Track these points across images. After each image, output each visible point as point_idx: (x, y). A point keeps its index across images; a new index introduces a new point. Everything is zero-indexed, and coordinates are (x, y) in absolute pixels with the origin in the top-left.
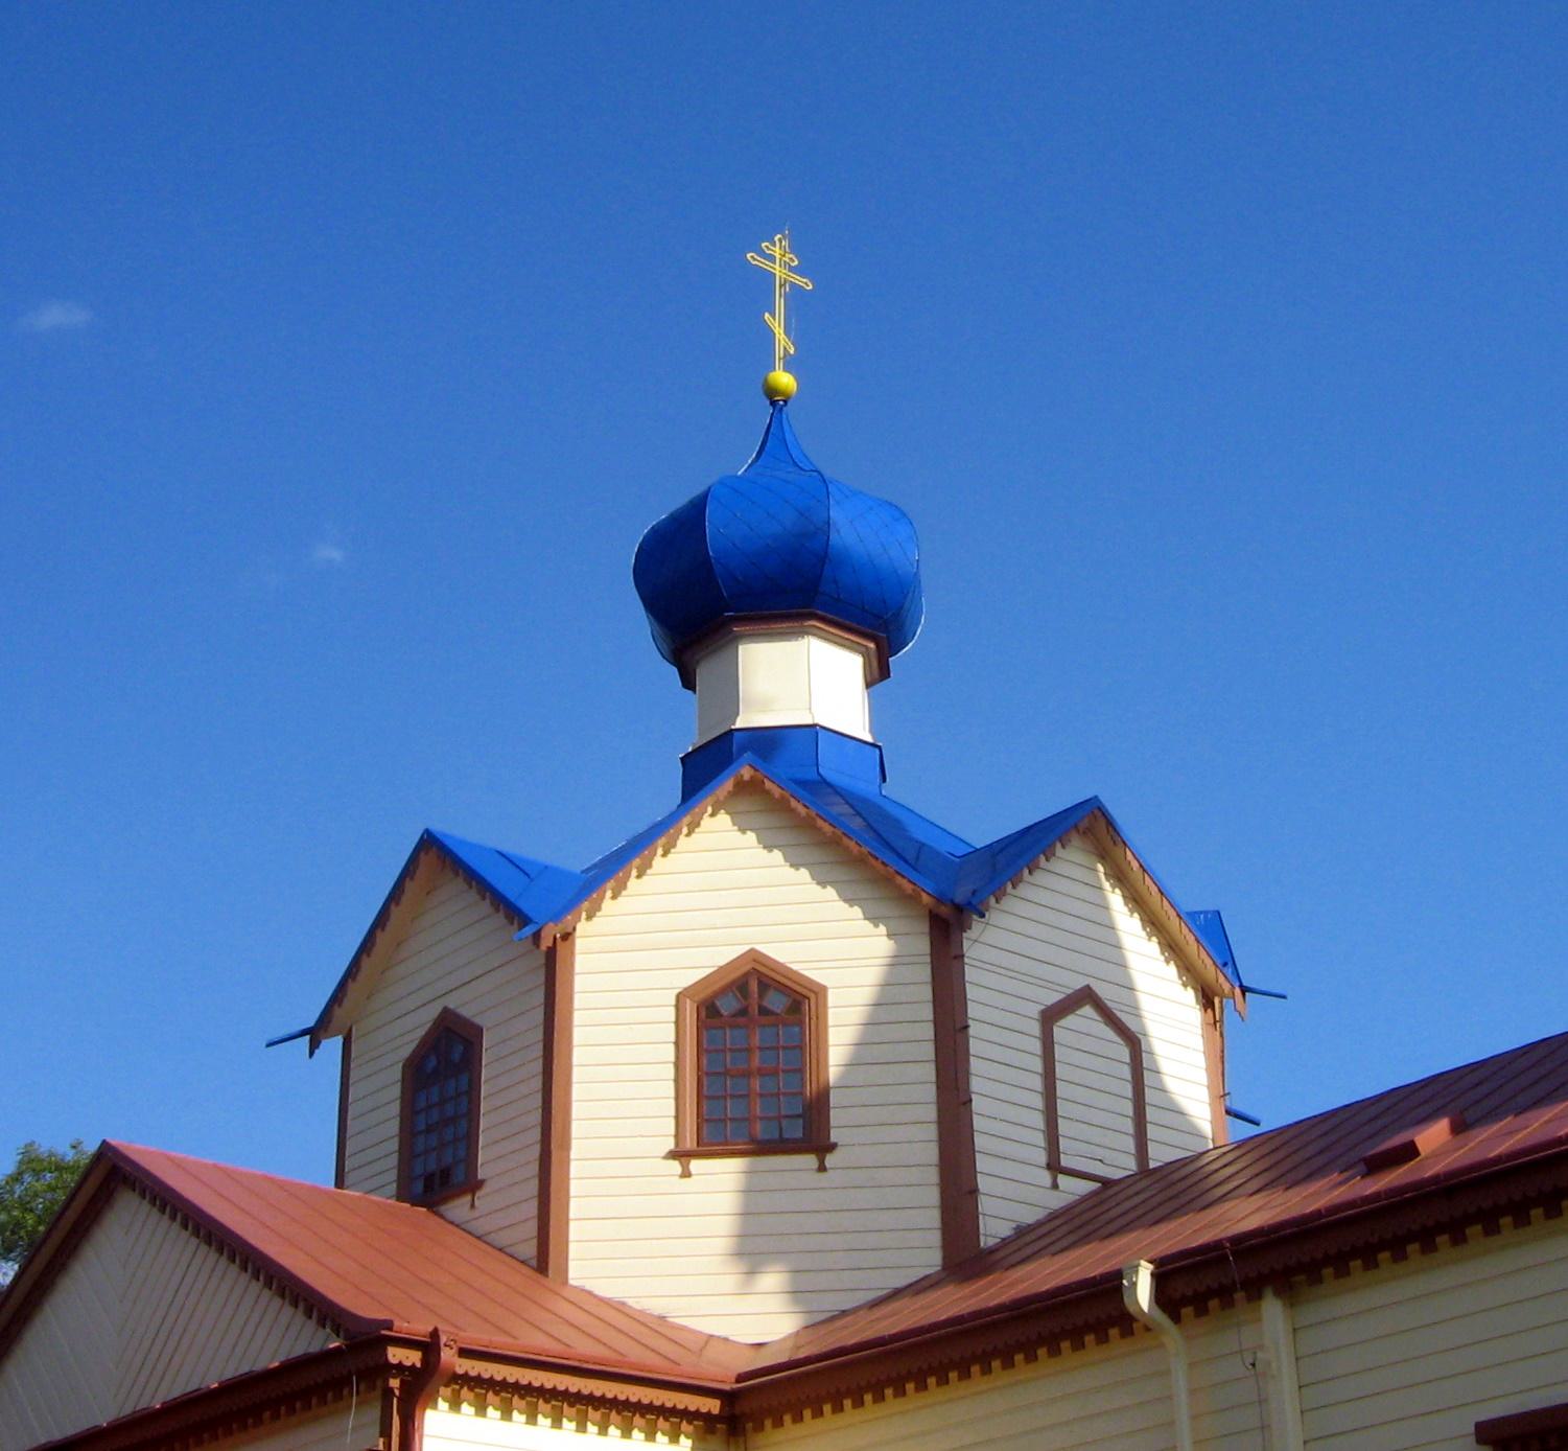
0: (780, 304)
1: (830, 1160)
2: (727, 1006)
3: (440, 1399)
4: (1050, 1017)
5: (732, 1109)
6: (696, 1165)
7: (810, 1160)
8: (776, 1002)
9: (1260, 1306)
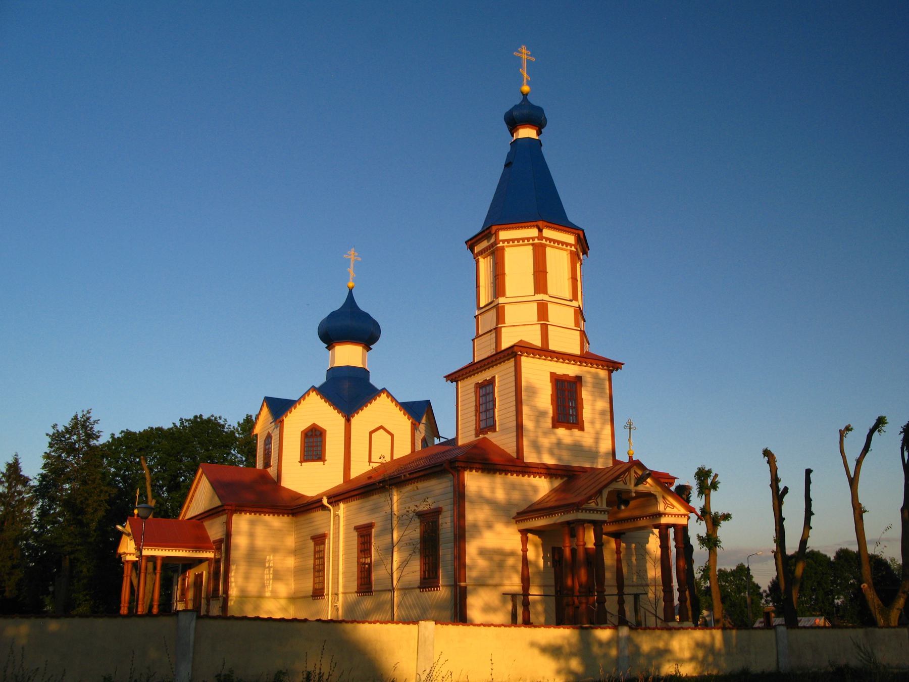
0: (352, 265)
1: (325, 462)
2: (310, 434)
3: (351, 478)
4: (371, 433)
5: (310, 453)
6: (303, 464)
7: (322, 463)
8: (318, 433)
9: (607, 402)
